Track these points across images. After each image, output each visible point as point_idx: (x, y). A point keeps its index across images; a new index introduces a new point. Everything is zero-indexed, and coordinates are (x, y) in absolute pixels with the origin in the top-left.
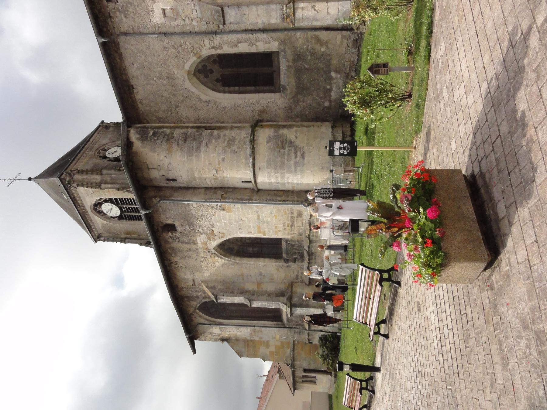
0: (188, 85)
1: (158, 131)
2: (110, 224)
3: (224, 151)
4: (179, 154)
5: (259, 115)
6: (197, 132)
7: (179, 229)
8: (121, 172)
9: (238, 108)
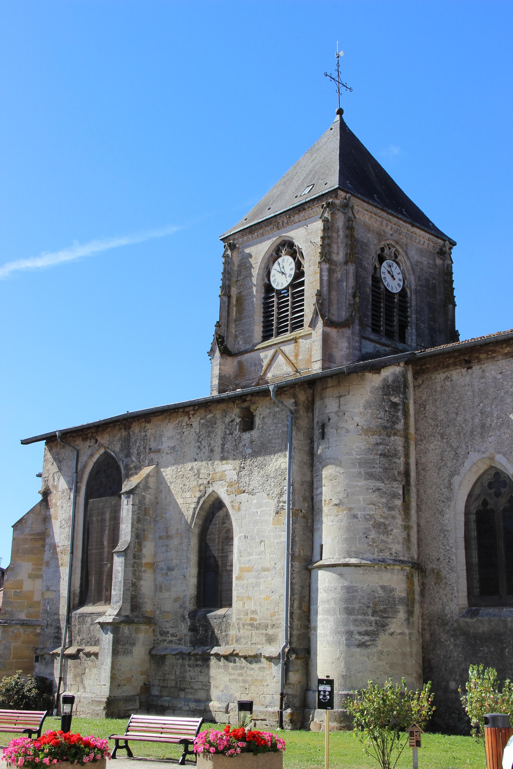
1: (399, 410)
3: (368, 518)
5: (433, 570)
6: (399, 473)
7: (246, 436)
8: (351, 298)
9: (442, 535)
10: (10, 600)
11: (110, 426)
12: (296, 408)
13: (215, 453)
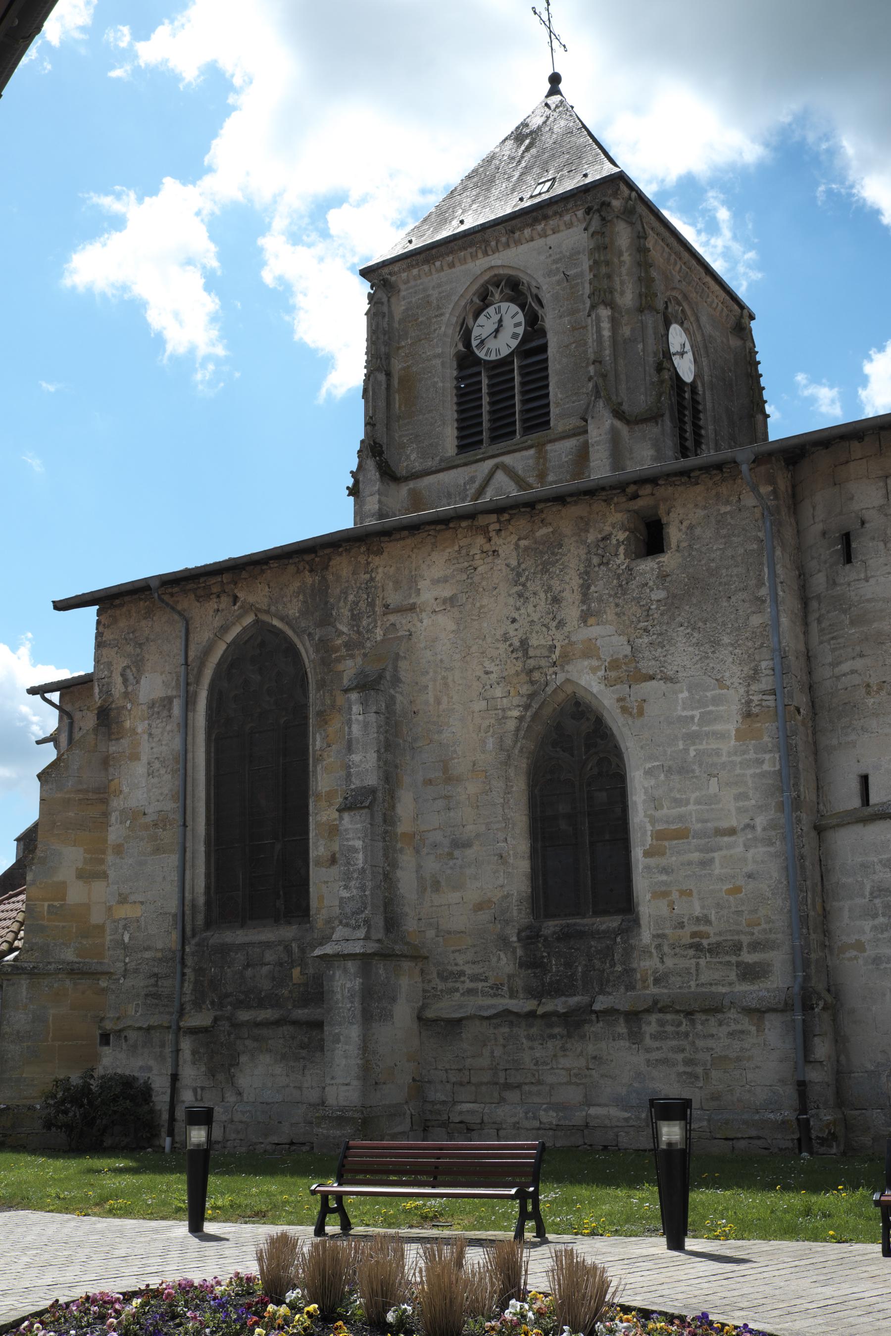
7: (648, 566)
8: (653, 372)
10: (40, 922)
11: (270, 568)
12: (776, 502)
13: (564, 604)
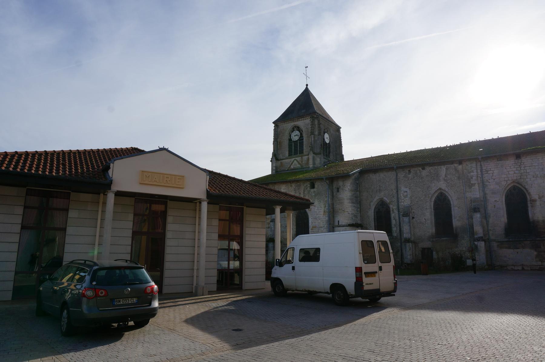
0: (377, 198)
2: (287, 134)
3: (352, 214)
4: (350, 194)
7: (312, 190)
